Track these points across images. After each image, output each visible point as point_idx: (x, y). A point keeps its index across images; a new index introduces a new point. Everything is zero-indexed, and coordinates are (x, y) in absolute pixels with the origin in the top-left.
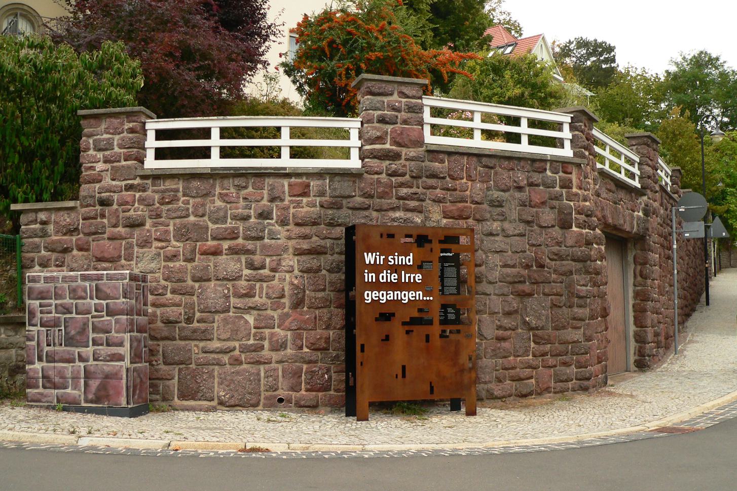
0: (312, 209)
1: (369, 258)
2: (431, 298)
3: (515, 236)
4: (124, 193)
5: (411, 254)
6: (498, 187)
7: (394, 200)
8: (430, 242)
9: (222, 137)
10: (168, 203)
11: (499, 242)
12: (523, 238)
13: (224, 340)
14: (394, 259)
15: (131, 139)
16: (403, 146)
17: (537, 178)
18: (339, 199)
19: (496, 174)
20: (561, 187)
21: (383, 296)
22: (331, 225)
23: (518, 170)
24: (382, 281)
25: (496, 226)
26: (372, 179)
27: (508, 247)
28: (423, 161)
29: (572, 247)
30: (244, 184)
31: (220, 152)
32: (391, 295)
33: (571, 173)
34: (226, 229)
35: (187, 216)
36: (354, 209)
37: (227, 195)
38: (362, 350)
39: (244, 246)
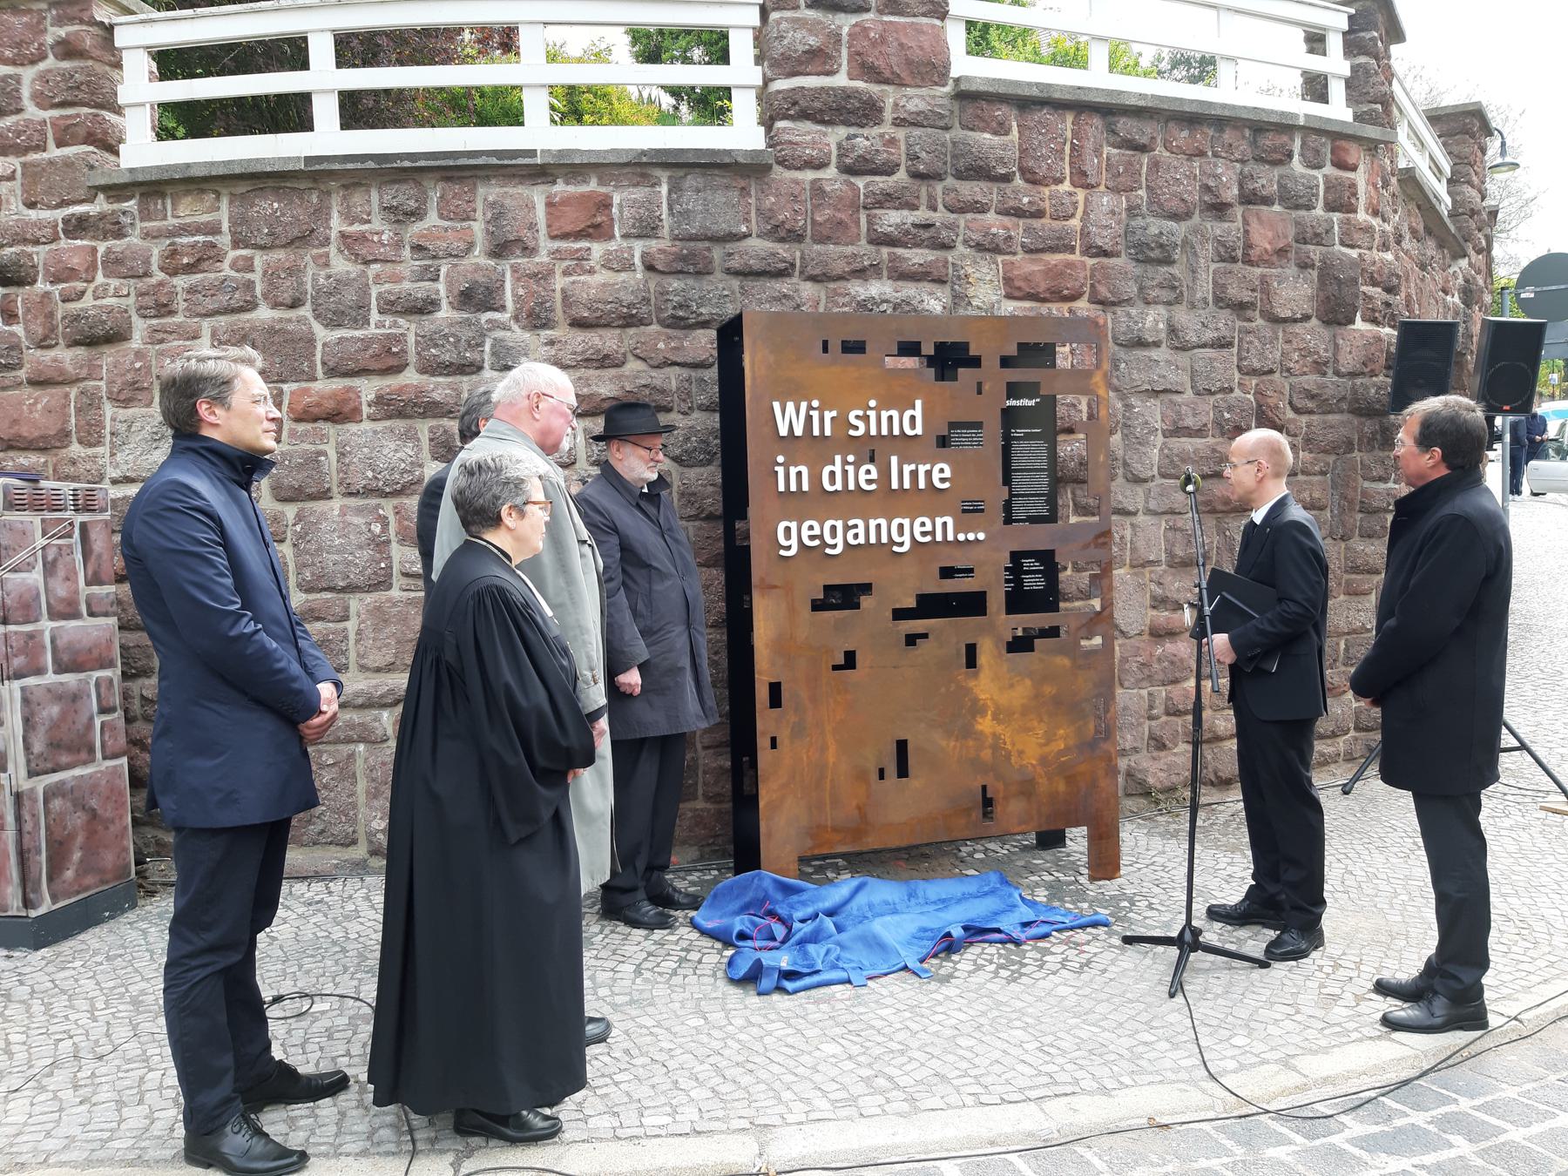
0: (623, 276)
1: (789, 418)
2: (981, 536)
3: (1204, 346)
4: (64, 243)
5: (918, 403)
6: (1160, 205)
7: (863, 247)
8: (975, 362)
9: (342, 61)
10: (191, 269)
11: (1165, 365)
12: (1225, 352)
13: (378, 670)
14: (866, 419)
15: (67, 76)
16: (887, 82)
17: (1267, 179)
18: (701, 245)
19: (1155, 165)
20: (1330, 207)
22: (678, 323)
23: (1215, 155)
24: (829, 488)
25: (1153, 320)
26: (797, 182)
27: (1186, 379)
28: (947, 128)
29: (1353, 375)
30: (413, 204)
31: (342, 106)
32: (862, 531)
33: (1354, 169)
34: (367, 342)
35: (250, 306)
37: (362, 238)
39: (420, 392)
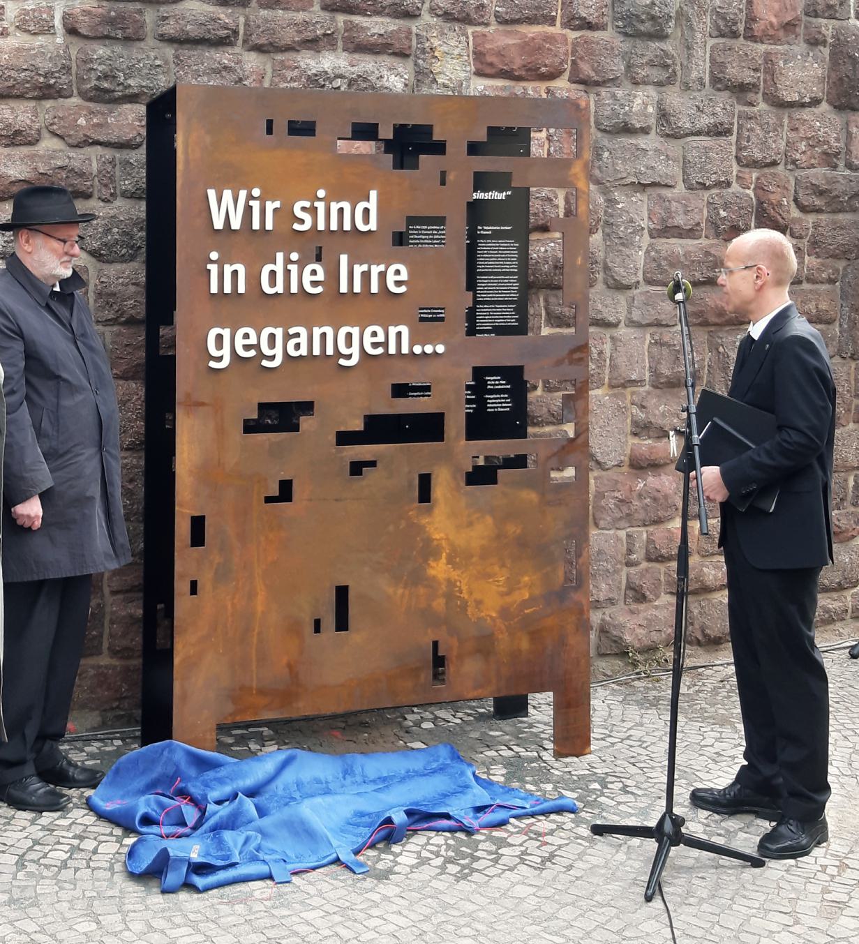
0: (41, 40)
1: (226, 209)
2: (440, 349)
5: (373, 194)
8: (439, 148)
12: (722, 140)
14: (313, 211)
21: (272, 344)
24: (267, 289)
27: (677, 170)
36: (181, 41)
38: (198, 537)
